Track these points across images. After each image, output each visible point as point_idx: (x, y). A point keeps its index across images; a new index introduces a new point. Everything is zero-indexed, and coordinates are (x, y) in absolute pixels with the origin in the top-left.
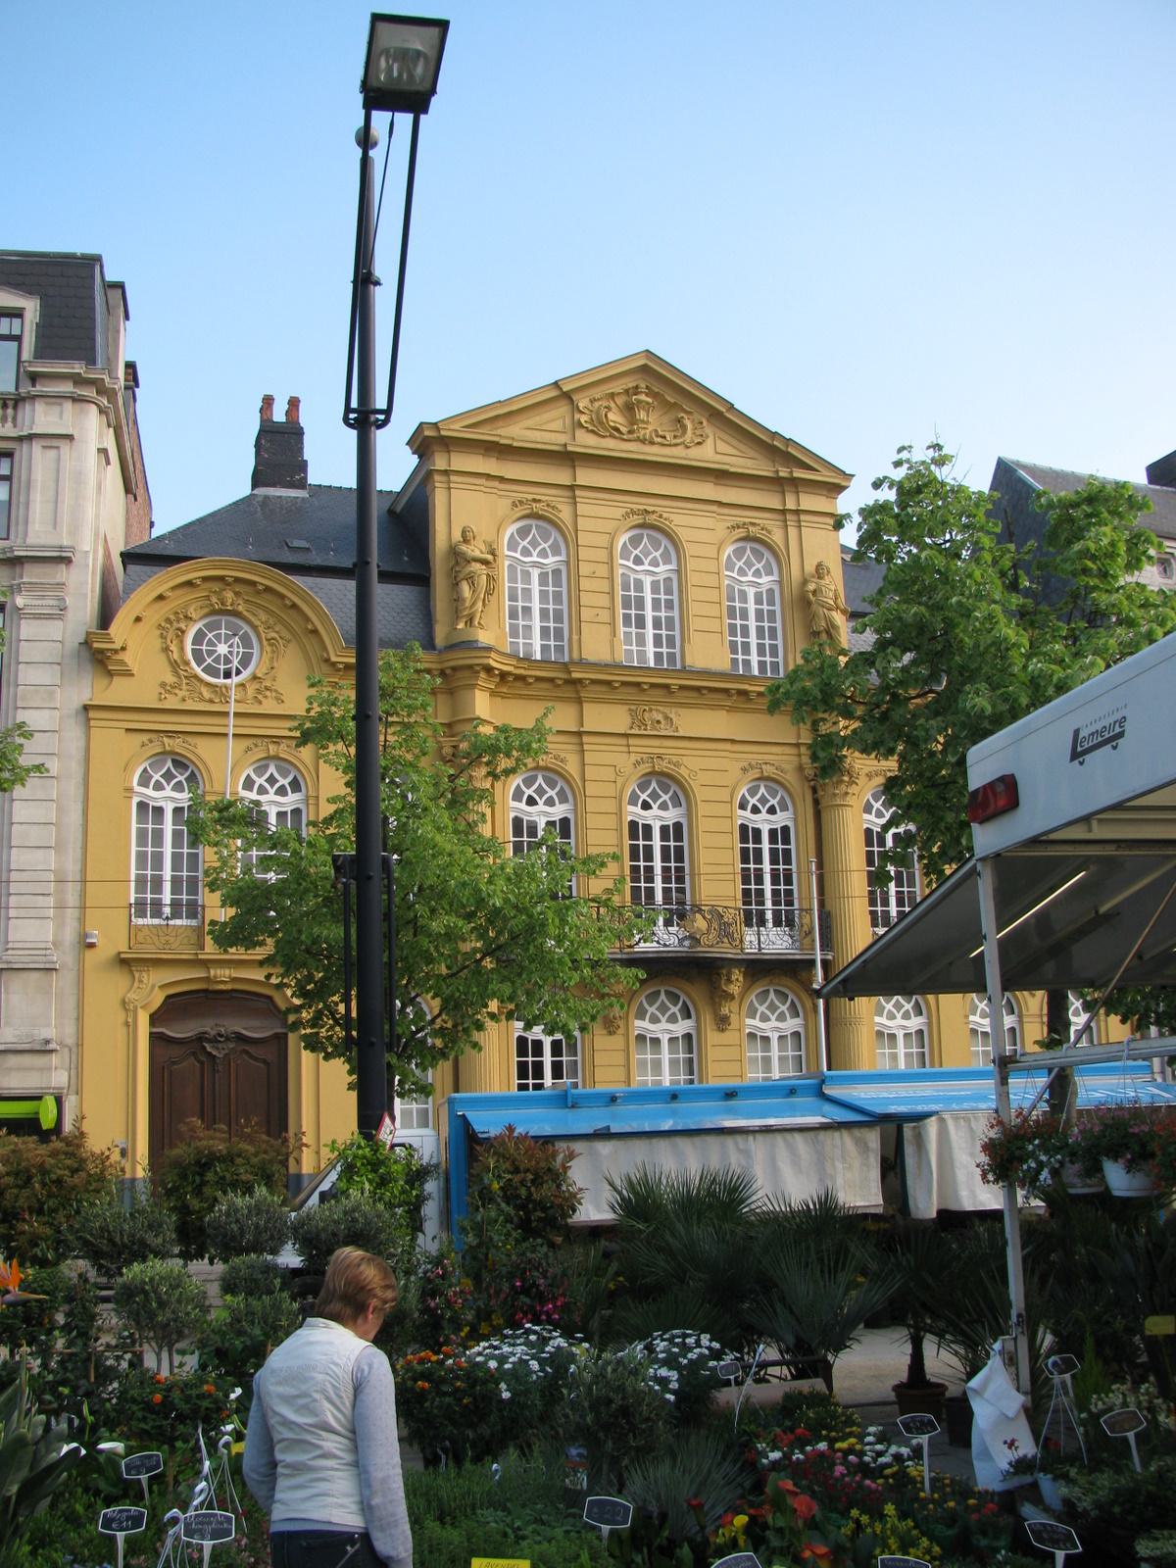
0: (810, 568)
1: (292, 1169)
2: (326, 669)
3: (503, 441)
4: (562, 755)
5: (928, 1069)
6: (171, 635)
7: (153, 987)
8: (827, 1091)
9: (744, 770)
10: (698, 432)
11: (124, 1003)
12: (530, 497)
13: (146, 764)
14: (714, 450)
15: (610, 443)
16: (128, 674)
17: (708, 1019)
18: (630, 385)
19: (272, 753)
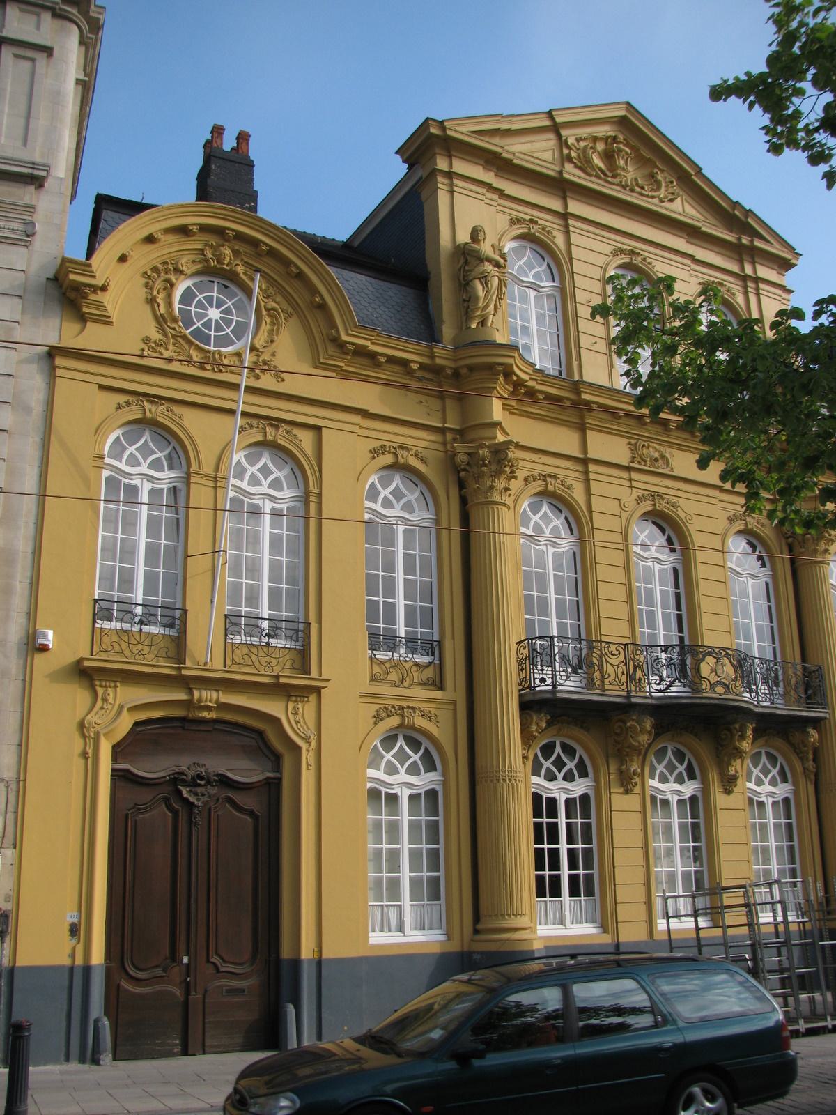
1: (286, 953)
2: (332, 350)
3: (505, 155)
4: (569, 482)
6: (158, 285)
7: (121, 708)
9: (731, 520)
10: (671, 190)
11: (81, 726)
13: (118, 433)
14: (683, 208)
16: (106, 321)
17: (714, 777)
18: (610, 134)
19: (269, 437)
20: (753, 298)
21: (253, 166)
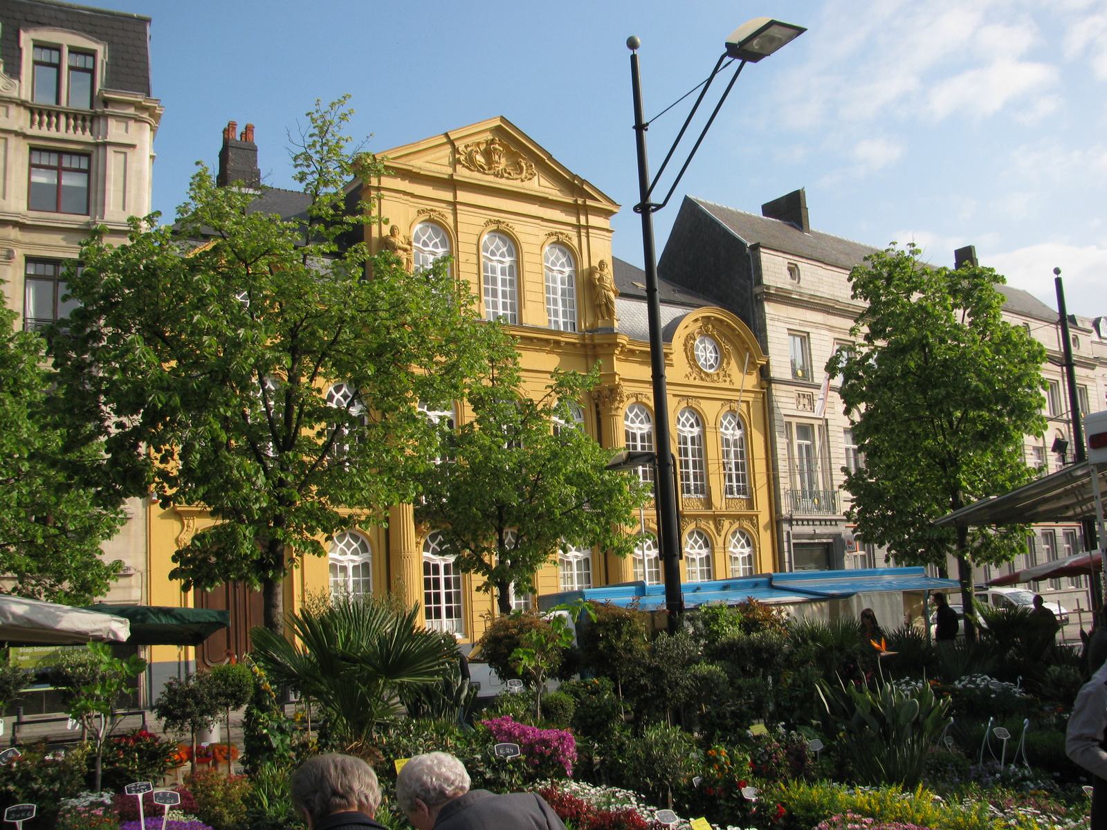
0: (595, 263)
3: (415, 170)
5: (868, 569)
8: (774, 584)
12: (429, 208)
14: (539, 185)
15: (477, 175)
20: (584, 239)
21: (256, 150)
